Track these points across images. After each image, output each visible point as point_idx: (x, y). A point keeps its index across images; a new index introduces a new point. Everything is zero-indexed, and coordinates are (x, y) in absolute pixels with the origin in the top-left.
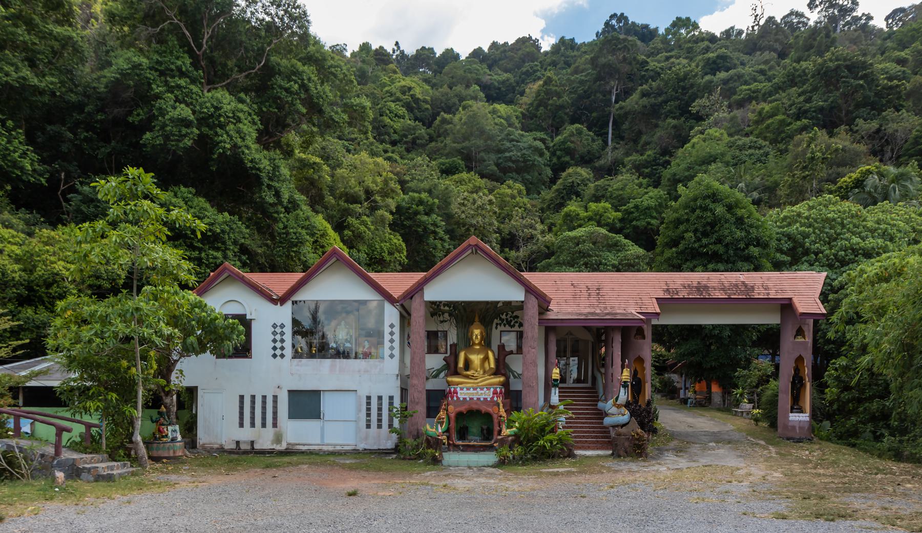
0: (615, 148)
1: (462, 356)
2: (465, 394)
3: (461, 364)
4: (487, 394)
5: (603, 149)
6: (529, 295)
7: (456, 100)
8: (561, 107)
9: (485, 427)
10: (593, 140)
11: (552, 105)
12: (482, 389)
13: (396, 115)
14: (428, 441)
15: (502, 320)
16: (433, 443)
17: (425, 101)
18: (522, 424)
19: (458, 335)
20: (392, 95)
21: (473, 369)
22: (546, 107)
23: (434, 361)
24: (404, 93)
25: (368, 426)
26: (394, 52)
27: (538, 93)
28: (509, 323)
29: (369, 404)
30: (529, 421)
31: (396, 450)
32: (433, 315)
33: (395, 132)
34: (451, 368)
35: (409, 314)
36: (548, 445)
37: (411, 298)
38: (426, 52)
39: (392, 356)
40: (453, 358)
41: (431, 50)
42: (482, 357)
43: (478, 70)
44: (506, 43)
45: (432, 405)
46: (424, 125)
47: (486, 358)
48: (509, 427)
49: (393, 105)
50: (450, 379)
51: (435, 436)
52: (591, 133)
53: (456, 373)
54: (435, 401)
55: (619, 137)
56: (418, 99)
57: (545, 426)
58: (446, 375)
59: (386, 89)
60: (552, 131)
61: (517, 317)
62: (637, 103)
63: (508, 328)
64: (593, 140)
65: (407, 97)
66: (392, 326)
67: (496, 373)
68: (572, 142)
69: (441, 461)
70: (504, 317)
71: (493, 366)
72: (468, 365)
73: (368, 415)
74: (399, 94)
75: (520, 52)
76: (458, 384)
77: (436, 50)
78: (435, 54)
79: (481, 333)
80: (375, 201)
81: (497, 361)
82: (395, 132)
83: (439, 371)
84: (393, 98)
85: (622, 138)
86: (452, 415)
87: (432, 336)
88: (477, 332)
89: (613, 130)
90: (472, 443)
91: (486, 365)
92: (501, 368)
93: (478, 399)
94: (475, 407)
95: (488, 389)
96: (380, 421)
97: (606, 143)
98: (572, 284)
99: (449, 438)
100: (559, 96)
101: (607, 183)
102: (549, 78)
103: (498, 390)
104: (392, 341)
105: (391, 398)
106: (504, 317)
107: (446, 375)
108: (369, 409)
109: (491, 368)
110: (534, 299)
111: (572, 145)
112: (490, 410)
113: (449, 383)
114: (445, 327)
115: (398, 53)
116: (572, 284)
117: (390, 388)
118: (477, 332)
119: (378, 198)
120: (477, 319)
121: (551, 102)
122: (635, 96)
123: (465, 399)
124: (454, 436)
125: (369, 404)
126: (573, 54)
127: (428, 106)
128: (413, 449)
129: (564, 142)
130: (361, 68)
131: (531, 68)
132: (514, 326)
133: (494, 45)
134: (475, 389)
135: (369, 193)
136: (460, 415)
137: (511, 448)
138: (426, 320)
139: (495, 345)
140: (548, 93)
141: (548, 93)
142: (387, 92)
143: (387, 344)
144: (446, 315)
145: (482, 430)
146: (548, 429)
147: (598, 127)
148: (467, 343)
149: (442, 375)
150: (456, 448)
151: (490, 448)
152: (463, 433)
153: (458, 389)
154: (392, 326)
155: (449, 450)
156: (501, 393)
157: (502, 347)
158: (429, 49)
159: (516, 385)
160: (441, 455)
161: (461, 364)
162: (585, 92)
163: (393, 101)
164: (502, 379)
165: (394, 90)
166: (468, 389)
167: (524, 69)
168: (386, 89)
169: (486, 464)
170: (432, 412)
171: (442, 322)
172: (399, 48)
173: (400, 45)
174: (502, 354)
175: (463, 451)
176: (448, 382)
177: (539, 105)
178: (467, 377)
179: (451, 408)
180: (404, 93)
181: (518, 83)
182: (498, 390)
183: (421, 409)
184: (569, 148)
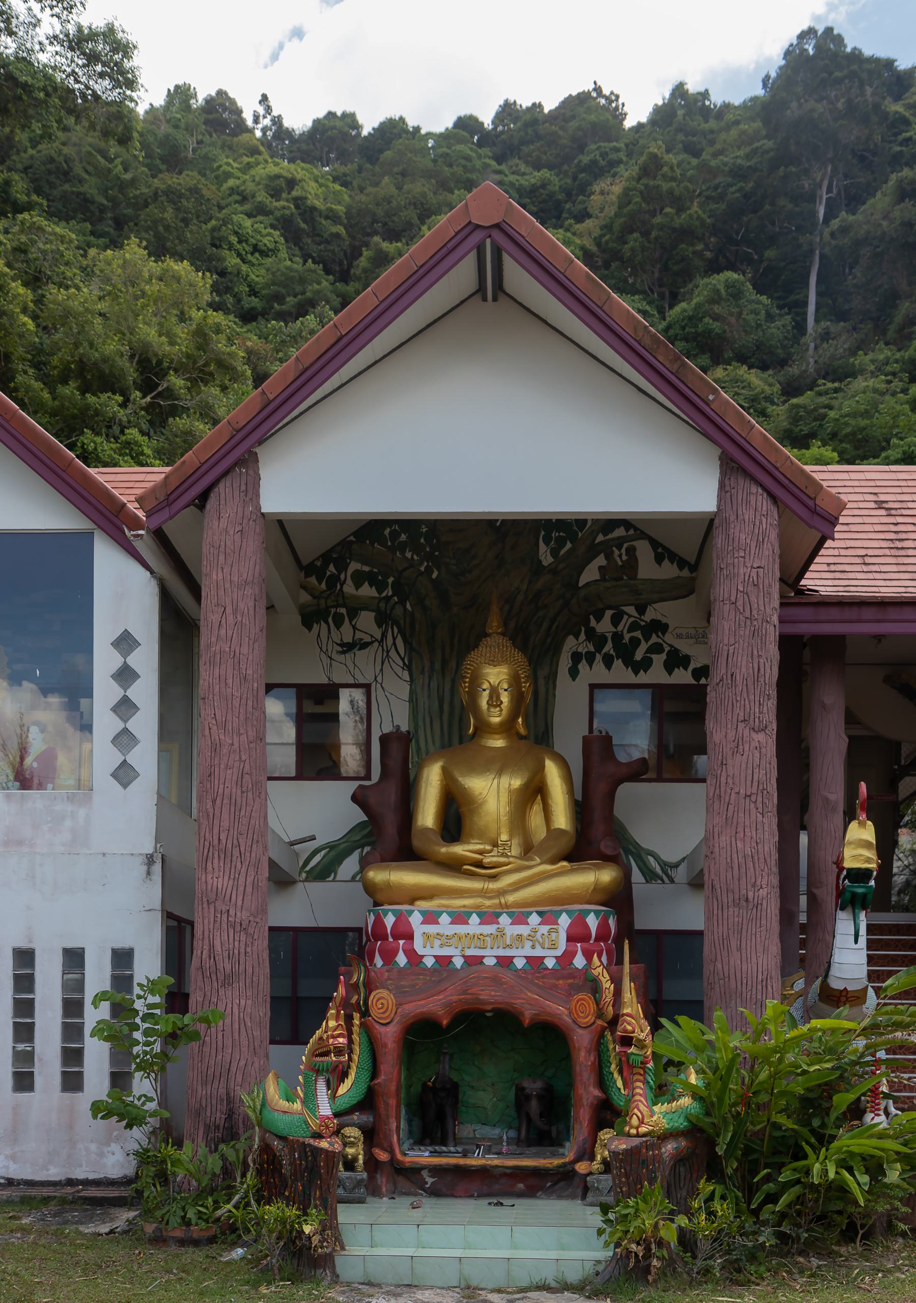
0: (825, 336)
1: (431, 781)
2: (446, 940)
3: (428, 814)
4: (543, 941)
5: (796, 340)
6: (742, 486)
7: (411, 214)
8: (686, 234)
9: (533, 1086)
10: (770, 317)
11: (661, 227)
12: (520, 919)
13: (255, 249)
14: (269, 1163)
15: (599, 641)
16: (297, 1174)
17: (332, 217)
18: (719, 1076)
19: (413, 700)
20: (244, 199)
21: (482, 836)
22: (646, 234)
23: (315, 812)
24: (275, 194)
25: (24, 1081)
26: (256, 120)
27: (625, 199)
28: (625, 652)
29: (24, 982)
30: (753, 1063)
31: (143, 1191)
32: (309, 619)
33: (253, 292)
34: (387, 831)
35: (195, 590)
36: (858, 1183)
37: (202, 500)
38: (338, 124)
39: (124, 774)
40: (392, 794)
41: (350, 119)
42: (517, 783)
43: (468, 159)
44: (537, 106)
45: (307, 988)
46: (327, 271)
47: (536, 790)
48: (661, 1092)
49: (248, 223)
50: (377, 875)
51: (298, 1134)
52: (764, 299)
53: (407, 852)
54: (311, 975)
55: (832, 309)
56: (313, 209)
57: (828, 1089)
58: (365, 864)
59: (231, 182)
60: (662, 296)
61: (659, 627)
62: (885, 217)
63: (621, 673)
64: (770, 317)
65: (283, 205)
66: (125, 643)
67: (579, 850)
68: (716, 318)
69: (327, 1261)
70: (604, 626)
71: (562, 820)
72: (456, 817)
73: (24, 1032)
74: (262, 196)
75: (574, 124)
76: (414, 896)
77: (361, 119)
78: (357, 126)
79: (515, 682)
80: (169, 393)
81: (581, 809)
82: (253, 292)
83: (336, 853)
84: (247, 207)
85: (841, 316)
86: (389, 1034)
87: (315, 709)
88: (496, 676)
89: (819, 294)
90: (475, 1161)
91: (536, 819)
92: (593, 836)
93: (505, 962)
94: (490, 996)
95: (548, 918)
96: (73, 1056)
97: (800, 327)
98: (880, 505)
99: (371, 1136)
100: (680, 204)
101: (823, 400)
102: (654, 157)
103: (592, 922)
104: (125, 708)
105: (122, 958)
106: (604, 626)
107: (365, 864)
108: (24, 1008)
109: (554, 834)
110: (763, 503)
111: (716, 326)
112: (558, 1010)
113: (377, 896)
114: (365, 665)
115: (267, 122)
116: (880, 505)
117: (120, 918)
118: (496, 676)
119: (177, 382)
120: (494, 624)
121: (658, 219)
122: (880, 201)
123: (444, 961)
124: (397, 1126)
125: (24, 982)
126: (706, 126)
127: (341, 229)
128: (202, 1194)
129: (693, 319)
130: (167, 136)
131: (604, 155)
132: (646, 664)
133: (508, 110)
134: (489, 918)
135: (150, 370)
136: (421, 1034)
137: (678, 1195)
138: (273, 635)
139: (569, 733)
140: (648, 195)
141: (648, 195)
142: (232, 191)
143: (105, 723)
144: (366, 620)
145: (522, 1098)
146: (842, 1100)
147: (782, 285)
148: (455, 729)
149: (350, 865)
150: (405, 1180)
151: (563, 1182)
152: (434, 1116)
153: (415, 919)
154: (125, 643)
155: (375, 1191)
156: (603, 934)
157: (598, 747)
158: (345, 115)
159: (670, 911)
160: (330, 1227)
161: (428, 814)
162: (746, 196)
163: (249, 215)
164: (606, 876)
165: (250, 187)
166: (460, 918)
167: (585, 159)
168: (231, 182)
169: (549, 1275)
170: (293, 1018)
171: (347, 648)
172: (268, 109)
173: (272, 102)
174: (602, 776)
175: (435, 1193)
176: (370, 889)
177: (628, 229)
178: (454, 866)
179: (382, 1001)
180: (275, 194)
181: (569, 194)
182: (592, 922)
183: (240, 1005)
184: (708, 332)
